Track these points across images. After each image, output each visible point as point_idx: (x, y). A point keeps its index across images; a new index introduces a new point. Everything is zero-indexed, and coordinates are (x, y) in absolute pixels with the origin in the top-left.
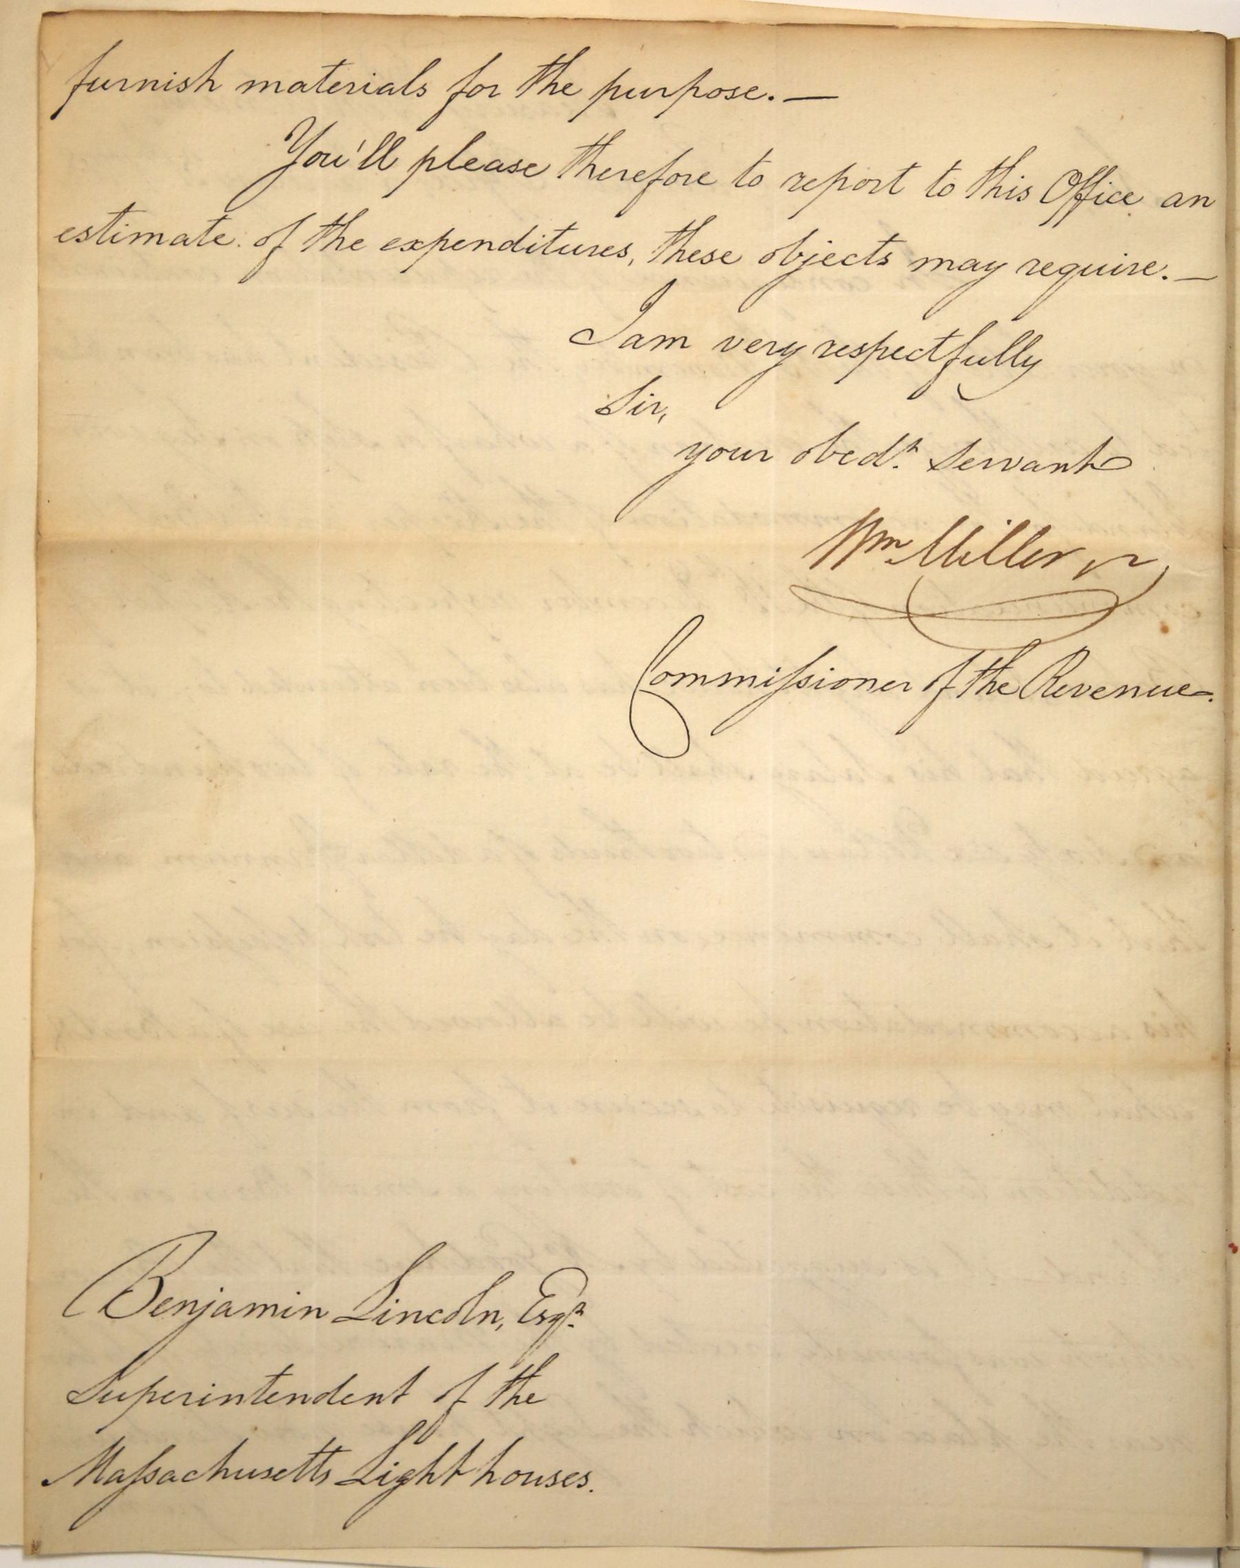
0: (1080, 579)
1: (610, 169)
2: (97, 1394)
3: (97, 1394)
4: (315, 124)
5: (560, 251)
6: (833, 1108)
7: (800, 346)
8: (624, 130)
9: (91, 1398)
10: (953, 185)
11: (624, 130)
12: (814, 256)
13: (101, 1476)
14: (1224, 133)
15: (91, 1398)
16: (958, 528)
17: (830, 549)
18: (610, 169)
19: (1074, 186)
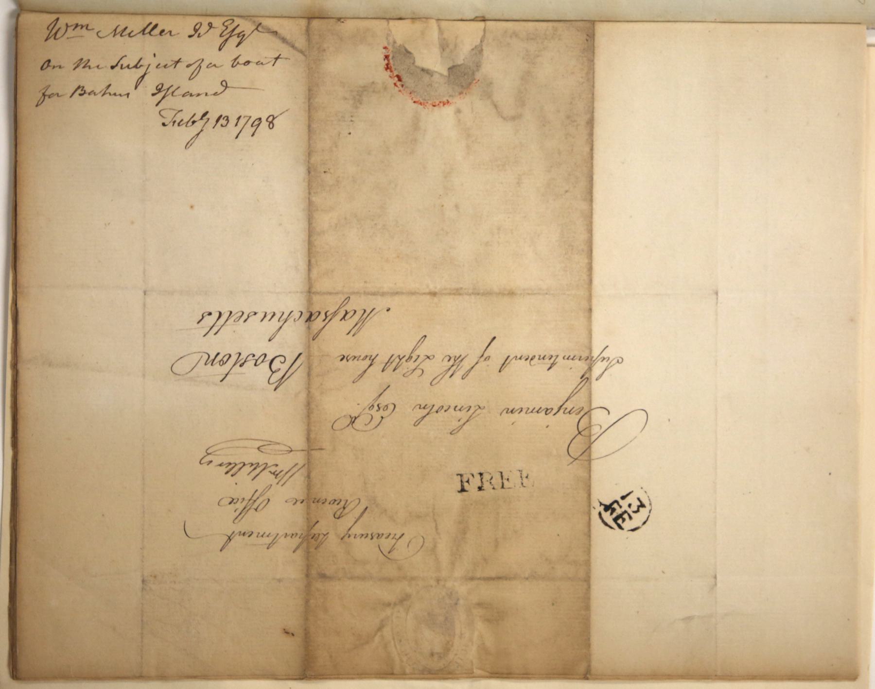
0: (240, 46)
1: (257, 490)
2: (369, 315)
3: (369, 315)
4: (268, 379)
5: (252, 465)
6: (191, 95)
7: (273, 319)
8: (270, 340)
9: (371, 312)
10: (286, 502)
11: (270, 340)
12: (256, 492)
13: (556, 361)
14: (18, 463)
15: (371, 312)
16: (356, 524)
17: (372, 313)
18: (257, 490)
19: (398, 539)
